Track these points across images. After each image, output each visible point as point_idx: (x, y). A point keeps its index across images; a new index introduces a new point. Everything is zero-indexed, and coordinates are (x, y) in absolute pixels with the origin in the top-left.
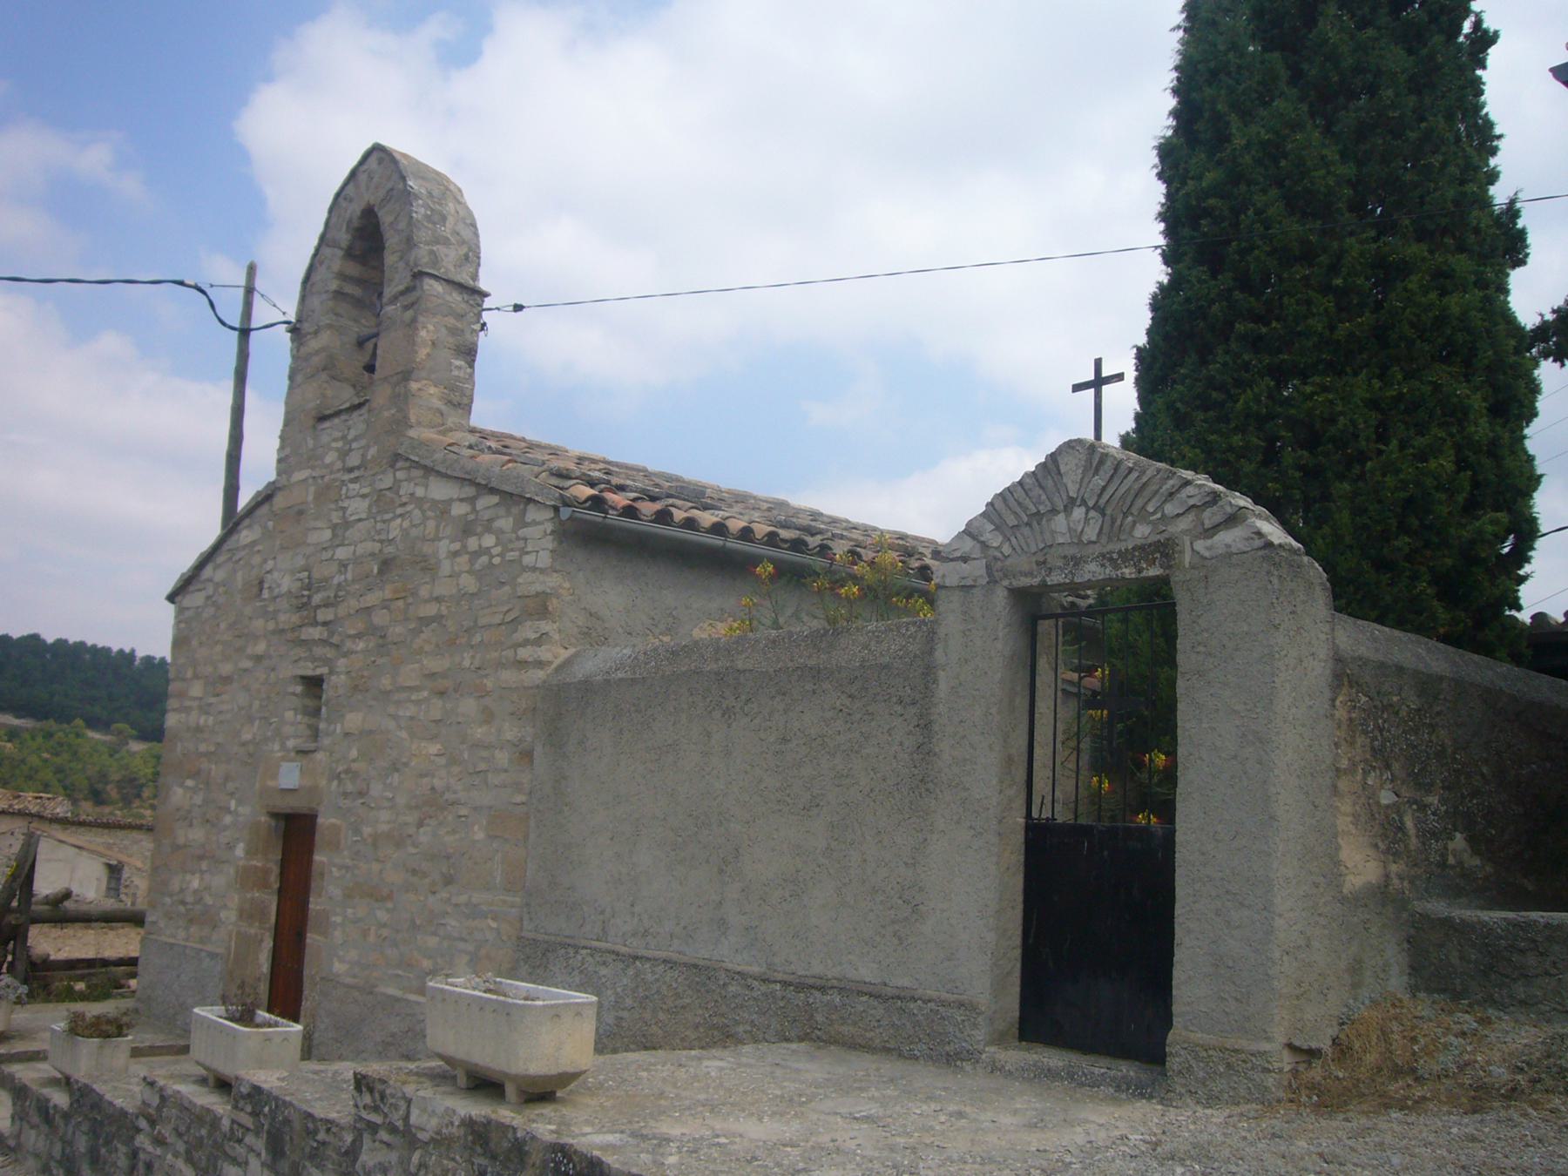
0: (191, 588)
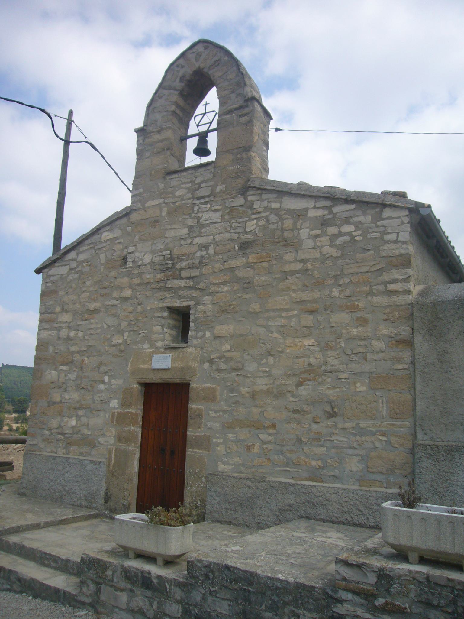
0: (57, 264)
